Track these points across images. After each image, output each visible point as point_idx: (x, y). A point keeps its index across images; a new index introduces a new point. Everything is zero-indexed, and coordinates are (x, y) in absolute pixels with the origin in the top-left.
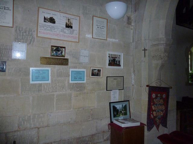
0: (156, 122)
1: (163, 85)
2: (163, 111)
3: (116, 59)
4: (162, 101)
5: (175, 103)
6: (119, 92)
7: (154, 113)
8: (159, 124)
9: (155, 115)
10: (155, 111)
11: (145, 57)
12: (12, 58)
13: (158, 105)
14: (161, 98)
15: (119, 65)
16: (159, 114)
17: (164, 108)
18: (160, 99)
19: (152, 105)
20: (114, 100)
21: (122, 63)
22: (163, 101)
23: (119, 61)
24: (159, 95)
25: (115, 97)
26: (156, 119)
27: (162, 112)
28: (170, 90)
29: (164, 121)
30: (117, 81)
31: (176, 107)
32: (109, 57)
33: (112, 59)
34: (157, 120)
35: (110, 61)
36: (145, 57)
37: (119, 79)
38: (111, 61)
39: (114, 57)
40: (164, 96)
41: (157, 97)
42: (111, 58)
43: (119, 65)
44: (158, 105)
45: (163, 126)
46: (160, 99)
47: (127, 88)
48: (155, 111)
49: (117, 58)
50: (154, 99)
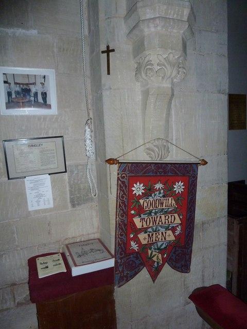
0: (151, 258)
1: (175, 156)
2: (174, 230)
3: (33, 89)
4: (171, 201)
5: (222, 199)
6: (53, 182)
7: (142, 237)
8: (163, 265)
9: (144, 242)
10: (144, 230)
11: (109, 73)
12: (57, 113)
13: (156, 213)
14: (168, 192)
15: (45, 105)
16: (160, 236)
17: (178, 221)
18: (164, 196)
19: (134, 216)
20: (38, 202)
21: (53, 99)
22: (173, 202)
23: (44, 95)
24: (159, 186)
25: (40, 196)
26: (150, 252)
27: (170, 232)
28: (201, 169)
29: (180, 255)
30: (41, 152)
31: (225, 212)
32: (5, 82)
33: (18, 89)
34: (154, 253)
35: (9, 94)
36: (109, 73)
37: (48, 144)
38: (14, 96)
39: (26, 81)
40: (179, 187)
41: (149, 192)
42: (13, 85)
43: (45, 105)
44: (156, 213)
45: (174, 267)
46: (164, 196)
47: (80, 167)
48: (144, 230)
49: (34, 84)
50: (140, 197)
